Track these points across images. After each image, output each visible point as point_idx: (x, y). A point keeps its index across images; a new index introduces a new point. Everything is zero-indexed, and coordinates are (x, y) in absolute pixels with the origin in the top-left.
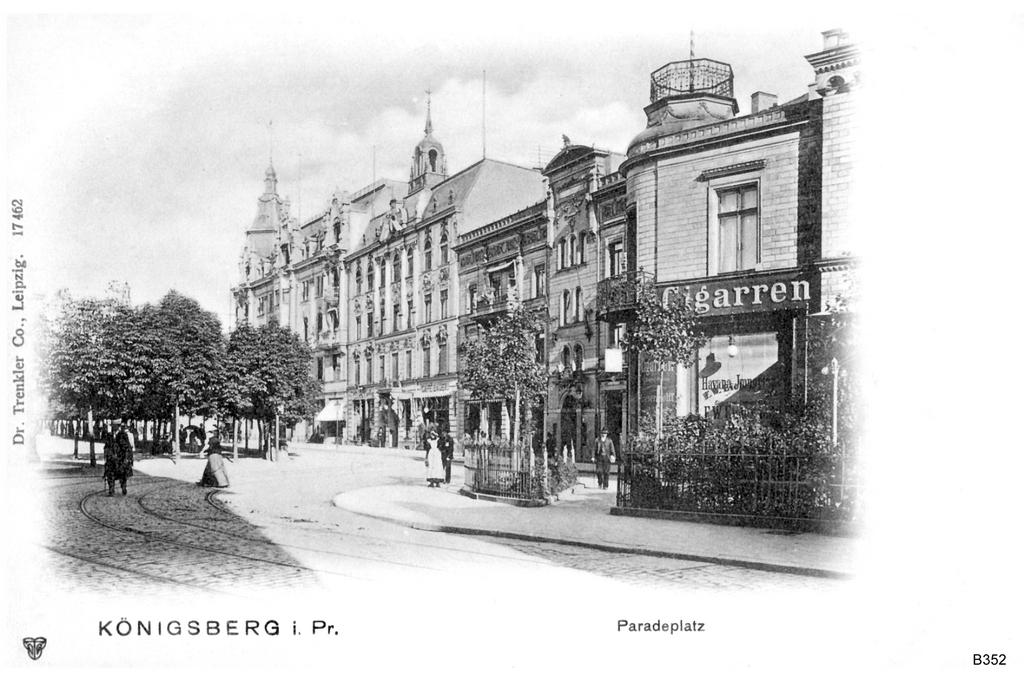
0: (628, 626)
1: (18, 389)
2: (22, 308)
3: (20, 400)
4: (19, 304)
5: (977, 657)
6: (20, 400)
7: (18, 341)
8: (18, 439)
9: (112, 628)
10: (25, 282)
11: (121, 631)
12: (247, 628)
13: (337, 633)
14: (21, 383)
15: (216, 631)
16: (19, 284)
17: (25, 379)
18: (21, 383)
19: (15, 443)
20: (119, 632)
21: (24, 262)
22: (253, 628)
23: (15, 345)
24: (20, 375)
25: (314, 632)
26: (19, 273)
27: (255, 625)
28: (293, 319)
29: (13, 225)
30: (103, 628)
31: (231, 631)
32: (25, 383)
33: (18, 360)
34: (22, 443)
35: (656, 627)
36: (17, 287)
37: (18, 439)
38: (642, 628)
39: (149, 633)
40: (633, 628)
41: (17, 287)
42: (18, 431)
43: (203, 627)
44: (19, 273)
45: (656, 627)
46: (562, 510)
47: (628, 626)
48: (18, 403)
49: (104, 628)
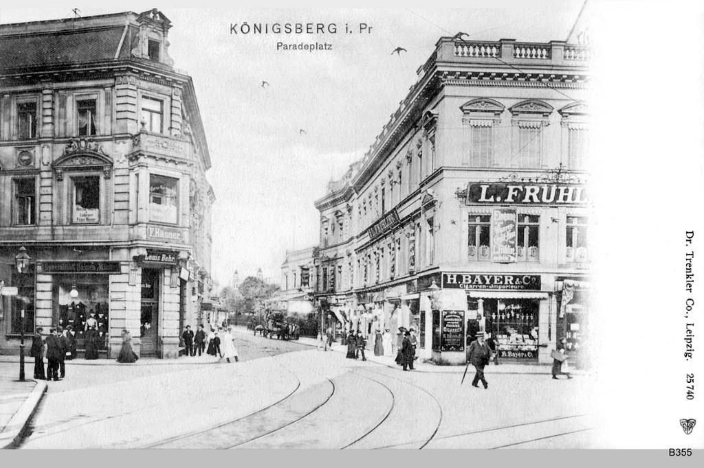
0: (283, 46)
1: (690, 269)
2: (688, 325)
3: (688, 262)
4: (689, 327)
5: (299, 26)
6: (688, 262)
7: (690, 303)
8: (690, 235)
9: (238, 29)
10: (685, 343)
11: (246, 27)
12: (318, 29)
13: (351, 32)
14: (688, 274)
15: (300, 31)
16: (689, 341)
17: (686, 277)
18: (688, 274)
19: (693, 232)
20: (242, 30)
21: (686, 356)
22: (321, 29)
23: (690, 299)
24: (689, 279)
25: (278, 49)
26: (689, 348)
27: (321, 26)
28: (538, 120)
29: (693, 389)
30: (233, 29)
31: (309, 31)
32: (685, 274)
33: (691, 289)
34: (687, 233)
35: (300, 47)
36: (691, 339)
37: (690, 235)
38: (292, 47)
39: (260, 32)
40: (286, 47)
41: (691, 339)
42: (690, 241)
43: (293, 27)
44: (689, 348)
45: (312, 47)
46: (184, 306)
47: (283, 46)
48: (690, 259)
49: (233, 28)
